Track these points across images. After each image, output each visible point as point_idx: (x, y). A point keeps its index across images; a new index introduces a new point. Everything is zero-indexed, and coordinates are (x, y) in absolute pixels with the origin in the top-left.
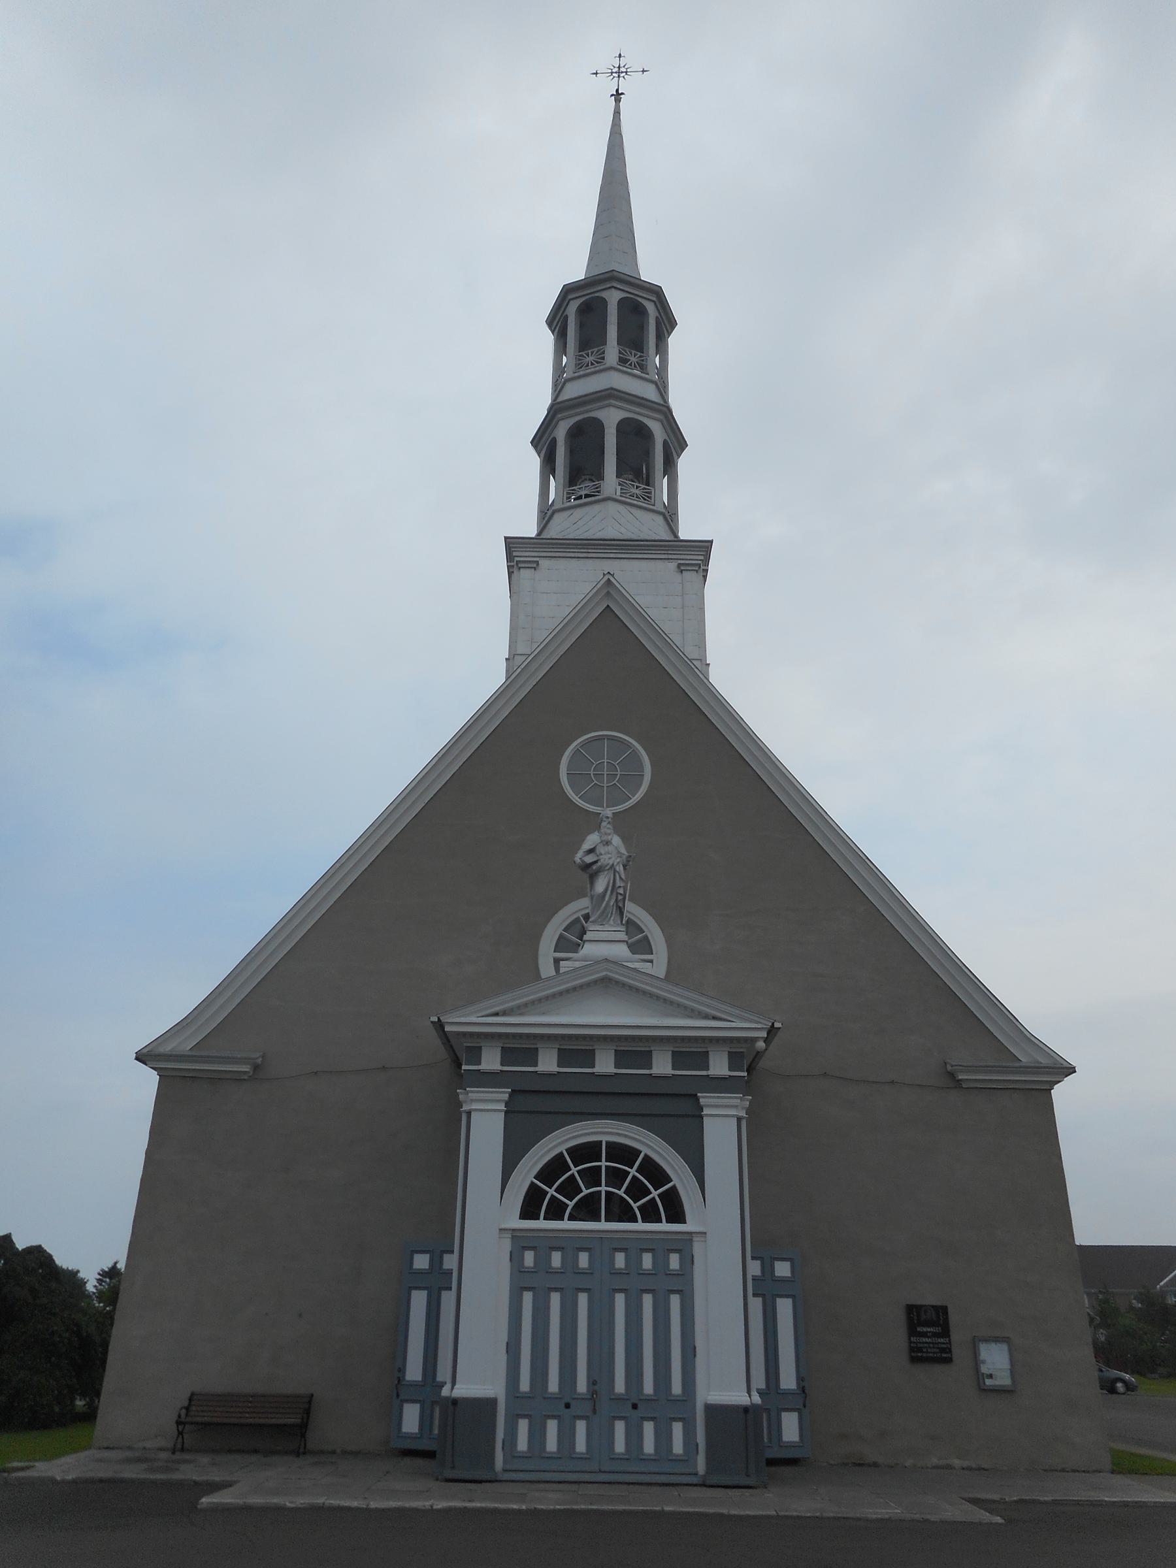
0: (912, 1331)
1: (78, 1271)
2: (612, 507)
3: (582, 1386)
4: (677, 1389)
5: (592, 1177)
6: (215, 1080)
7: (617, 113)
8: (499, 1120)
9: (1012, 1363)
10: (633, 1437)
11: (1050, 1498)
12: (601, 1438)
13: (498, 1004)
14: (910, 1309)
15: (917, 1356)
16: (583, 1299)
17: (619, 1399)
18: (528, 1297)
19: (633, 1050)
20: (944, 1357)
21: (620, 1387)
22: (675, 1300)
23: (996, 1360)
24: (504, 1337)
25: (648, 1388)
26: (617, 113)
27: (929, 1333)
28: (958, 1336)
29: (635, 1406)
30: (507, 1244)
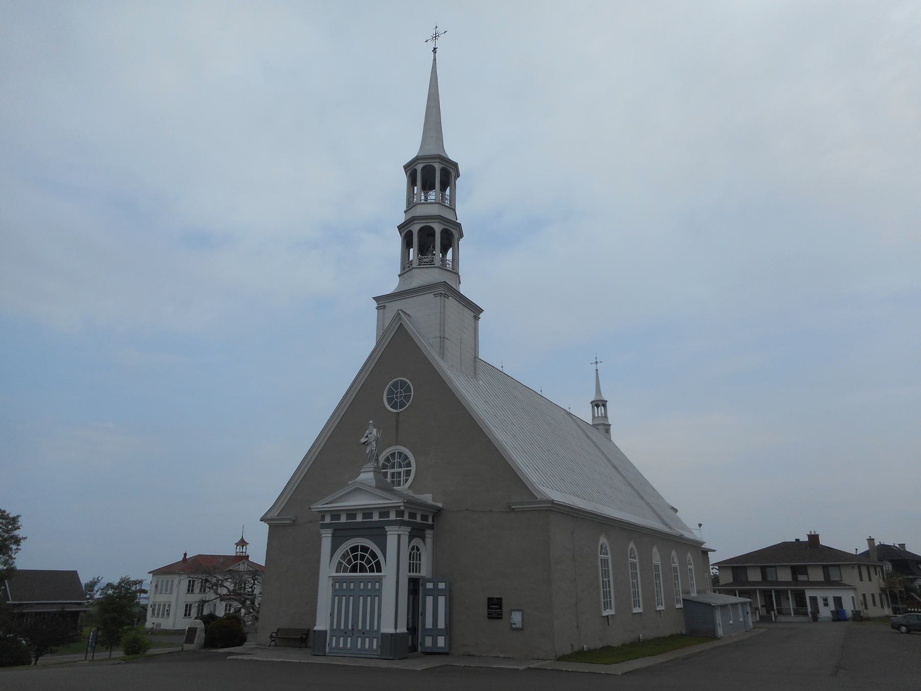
0: (489, 608)
1: (903, 546)
2: (436, 270)
3: (350, 627)
4: (375, 628)
5: (355, 558)
6: (284, 526)
7: (435, 60)
8: (330, 540)
9: (523, 619)
10: (363, 643)
11: (524, 667)
12: (354, 643)
13: (329, 499)
14: (490, 599)
15: (491, 617)
16: (351, 598)
17: (359, 631)
18: (337, 598)
19: (367, 513)
20: (499, 617)
21: (360, 628)
22: (377, 598)
23: (517, 618)
24: (329, 612)
25: (368, 628)
26: (435, 60)
27: (495, 607)
28: (505, 609)
29: (364, 633)
30: (331, 582)
